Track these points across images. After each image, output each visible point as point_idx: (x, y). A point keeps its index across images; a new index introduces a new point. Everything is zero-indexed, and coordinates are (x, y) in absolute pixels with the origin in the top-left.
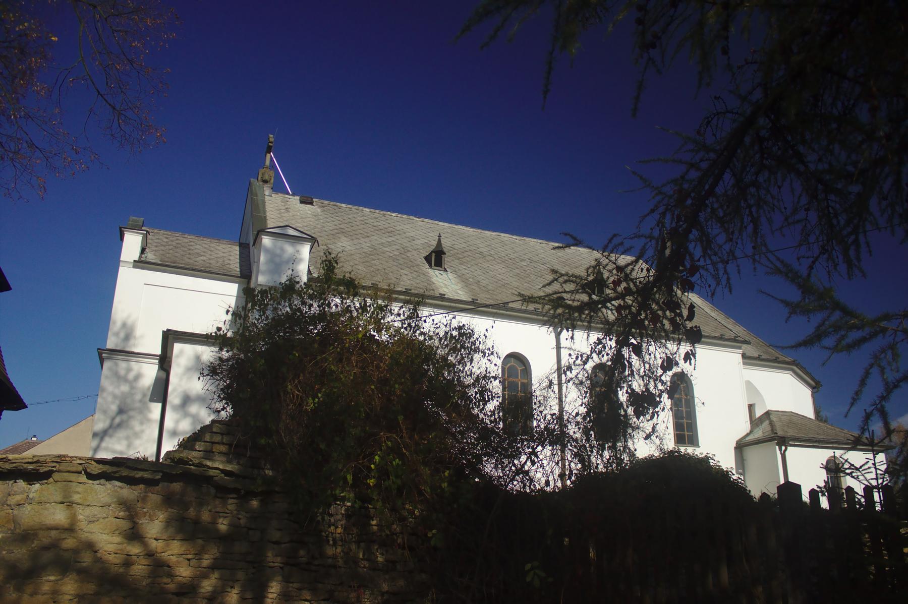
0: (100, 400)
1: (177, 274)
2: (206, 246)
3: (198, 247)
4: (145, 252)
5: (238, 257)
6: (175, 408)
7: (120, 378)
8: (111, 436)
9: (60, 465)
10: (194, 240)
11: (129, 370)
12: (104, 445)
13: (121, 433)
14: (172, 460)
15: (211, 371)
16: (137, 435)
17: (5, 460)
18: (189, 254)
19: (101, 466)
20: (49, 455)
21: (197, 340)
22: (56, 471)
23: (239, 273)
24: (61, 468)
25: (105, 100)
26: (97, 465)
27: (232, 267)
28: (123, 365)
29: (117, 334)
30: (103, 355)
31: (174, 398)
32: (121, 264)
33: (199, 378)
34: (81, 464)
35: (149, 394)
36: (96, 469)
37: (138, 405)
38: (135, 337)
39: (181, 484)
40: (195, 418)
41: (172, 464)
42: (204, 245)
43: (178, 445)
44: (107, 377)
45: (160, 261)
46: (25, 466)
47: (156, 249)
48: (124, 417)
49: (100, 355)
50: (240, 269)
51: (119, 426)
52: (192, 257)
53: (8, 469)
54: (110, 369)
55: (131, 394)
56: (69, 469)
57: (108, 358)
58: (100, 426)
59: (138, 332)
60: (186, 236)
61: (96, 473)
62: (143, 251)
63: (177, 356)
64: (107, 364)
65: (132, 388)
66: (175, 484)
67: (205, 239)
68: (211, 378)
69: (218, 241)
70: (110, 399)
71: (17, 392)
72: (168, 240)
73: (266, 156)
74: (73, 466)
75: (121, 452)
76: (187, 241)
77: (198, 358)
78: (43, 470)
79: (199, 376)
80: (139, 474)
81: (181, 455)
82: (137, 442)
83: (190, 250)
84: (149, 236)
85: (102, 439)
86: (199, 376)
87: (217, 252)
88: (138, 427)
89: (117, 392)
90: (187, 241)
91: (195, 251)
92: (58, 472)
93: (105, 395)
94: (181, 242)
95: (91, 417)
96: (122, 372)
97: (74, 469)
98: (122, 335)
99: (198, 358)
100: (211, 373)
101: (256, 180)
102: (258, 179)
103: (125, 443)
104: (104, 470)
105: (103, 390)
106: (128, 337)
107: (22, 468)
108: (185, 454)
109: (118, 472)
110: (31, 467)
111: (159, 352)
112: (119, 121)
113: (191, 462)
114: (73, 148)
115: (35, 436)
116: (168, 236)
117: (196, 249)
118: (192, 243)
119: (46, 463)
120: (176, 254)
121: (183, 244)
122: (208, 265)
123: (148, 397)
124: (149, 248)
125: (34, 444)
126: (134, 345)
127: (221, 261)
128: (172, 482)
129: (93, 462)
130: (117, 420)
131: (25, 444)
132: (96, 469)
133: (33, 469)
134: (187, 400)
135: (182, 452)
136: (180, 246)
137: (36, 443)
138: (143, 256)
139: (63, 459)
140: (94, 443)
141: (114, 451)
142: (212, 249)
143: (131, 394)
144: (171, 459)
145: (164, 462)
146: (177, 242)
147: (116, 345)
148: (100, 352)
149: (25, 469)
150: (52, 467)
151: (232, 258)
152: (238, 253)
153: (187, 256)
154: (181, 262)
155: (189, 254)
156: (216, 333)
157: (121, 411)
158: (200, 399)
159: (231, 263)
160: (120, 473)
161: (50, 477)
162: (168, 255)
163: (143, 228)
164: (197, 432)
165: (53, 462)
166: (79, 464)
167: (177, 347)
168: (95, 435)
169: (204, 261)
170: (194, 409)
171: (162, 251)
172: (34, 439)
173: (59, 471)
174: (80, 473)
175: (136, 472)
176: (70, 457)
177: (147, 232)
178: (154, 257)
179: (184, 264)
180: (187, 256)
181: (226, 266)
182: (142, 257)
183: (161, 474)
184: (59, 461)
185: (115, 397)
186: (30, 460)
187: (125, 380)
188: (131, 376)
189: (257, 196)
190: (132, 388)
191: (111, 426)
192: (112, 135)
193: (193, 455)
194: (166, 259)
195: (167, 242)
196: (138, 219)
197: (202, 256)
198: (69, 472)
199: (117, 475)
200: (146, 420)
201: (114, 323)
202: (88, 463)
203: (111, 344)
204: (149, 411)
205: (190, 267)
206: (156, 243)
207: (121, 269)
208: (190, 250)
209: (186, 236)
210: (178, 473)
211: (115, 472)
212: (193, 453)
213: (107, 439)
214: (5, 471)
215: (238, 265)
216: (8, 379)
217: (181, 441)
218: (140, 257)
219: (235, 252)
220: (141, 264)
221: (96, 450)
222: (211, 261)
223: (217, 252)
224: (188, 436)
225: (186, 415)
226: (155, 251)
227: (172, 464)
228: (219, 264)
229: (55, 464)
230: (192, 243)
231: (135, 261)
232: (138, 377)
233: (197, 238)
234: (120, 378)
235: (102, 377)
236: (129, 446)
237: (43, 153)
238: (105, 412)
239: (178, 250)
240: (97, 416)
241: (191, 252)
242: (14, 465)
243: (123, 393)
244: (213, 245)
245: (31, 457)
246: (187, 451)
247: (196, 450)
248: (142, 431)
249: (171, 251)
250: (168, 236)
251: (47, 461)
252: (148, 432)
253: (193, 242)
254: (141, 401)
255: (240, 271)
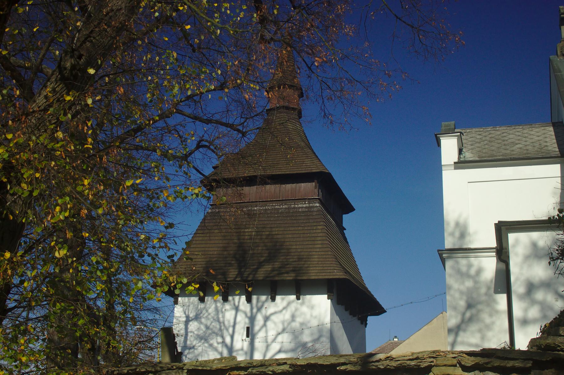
0: (448, 298)
1: (531, 165)
2: (519, 134)
3: (511, 136)
4: (462, 152)
5: (554, 137)
6: (522, 297)
7: (463, 275)
8: (465, 331)
9: (437, 360)
10: (506, 131)
11: (470, 266)
12: (459, 339)
13: (474, 327)
14: (539, 347)
15: (560, 254)
16: (488, 327)
17: (390, 358)
18: (505, 145)
19: (472, 358)
20: (425, 352)
21: (525, 227)
22: (434, 366)
23: (558, 153)
24: (438, 362)
25: (403, 22)
26: (469, 357)
27: (550, 148)
28: (463, 262)
29: (452, 234)
30: (444, 255)
31: (518, 287)
32: (443, 168)
33: (550, 263)
34: (455, 358)
35: (493, 286)
36: (469, 361)
37: (484, 298)
38: (469, 234)
39: (553, 370)
40: (544, 306)
41: (539, 351)
42: (517, 133)
43: (541, 332)
44: (450, 276)
45: (479, 158)
46: (408, 362)
47: (473, 147)
48: (474, 311)
49: (441, 255)
50: (559, 148)
51: (471, 319)
52: (508, 147)
53: (394, 366)
54: (453, 268)
55: (476, 288)
56: (445, 363)
57: (449, 258)
58: (453, 322)
59: (471, 229)
60: (498, 129)
61: (470, 365)
62: (460, 151)
63: (514, 246)
64: (449, 264)
65: (476, 282)
66: (546, 371)
67: (517, 127)
68: (562, 261)
69: (530, 126)
70: (457, 295)
71: (376, 299)
72: (481, 137)
73: (561, 29)
74: (448, 360)
75: (477, 346)
76: (499, 133)
77: (534, 245)
78: (423, 365)
79: (550, 260)
80: (510, 364)
81: (548, 342)
82: (490, 334)
83: (504, 141)
84: (463, 137)
85: (457, 334)
86: (550, 260)
87: (531, 137)
88: (488, 320)
89: (462, 288)
90: (499, 133)
91: (510, 141)
92: (436, 366)
93: (452, 292)
94: (494, 135)
95: (441, 314)
96: (464, 269)
97: (449, 363)
98: (457, 234)
99: (534, 245)
100: (560, 256)
101: (556, 56)
102: (557, 55)
103: (478, 336)
104: (477, 361)
105: (450, 288)
106: (463, 235)
107: (405, 365)
108: (550, 340)
109: (490, 363)
110: (413, 363)
111: (494, 244)
112: (419, 37)
113: (559, 348)
114: (385, 74)
115: (396, 337)
116: (480, 133)
117: (510, 139)
118: (505, 134)
119: (424, 359)
120: (492, 147)
121: (497, 137)
122: (525, 152)
123: (492, 290)
124: (465, 147)
125: (396, 345)
126: (470, 242)
127: (537, 145)
128: (543, 370)
129: (465, 355)
130: (468, 315)
131: (389, 345)
132: (469, 362)
133: (415, 365)
134: (531, 288)
135: (546, 338)
136: (493, 139)
137: (398, 343)
138: (461, 156)
139: (437, 354)
140: (451, 339)
141: (470, 345)
142: (526, 135)
143: (476, 288)
144: (537, 346)
145: (531, 350)
146: (490, 136)
147: (454, 244)
148: (441, 252)
149: (408, 365)
150: (430, 362)
151: (547, 140)
152: (553, 133)
153: (503, 147)
154: (498, 154)
155: (505, 145)
156: (558, 215)
157: (469, 306)
158: (546, 285)
159: (548, 144)
160: (492, 364)
161: (430, 371)
162: (484, 151)
163: (456, 130)
164: (558, 317)
165: (430, 357)
166: (453, 358)
167: (512, 237)
168: (450, 331)
169: (521, 148)
170: (539, 295)
171: (478, 148)
172: (396, 340)
173: (437, 366)
174: (455, 366)
175: (507, 361)
176: (443, 352)
177: (461, 133)
178: (472, 155)
179: (502, 155)
180: (503, 147)
181: (544, 148)
182: (461, 158)
183: (532, 362)
184: (435, 356)
185: (462, 293)
186: (411, 357)
187: (467, 275)
188: (473, 271)
189: (560, 71)
190: (476, 282)
191: (463, 321)
192: (416, 52)
193: (559, 341)
194: (484, 155)
195: (480, 139)
196: (449, 123)
197: (517, 144)
198: (445, 365)
199: (489, 366)
200: (495, 312)
201: (448, 224)
202: (461, 356)
203: (449, 243)
204: (495, 301)
205: (508, 157)
206: (471, 141)
207: (444, 173)
208: (504, 141)
209: (498, 129)
210: (548, 359)
211: (487, 363)
212: (559, 339)
213: (461, 334)
214: (393, 368)
215: (556, 145)
216: (366, 289)
217: (543, 327)
218: (459, 158)
219: (549, 133)
220: (461, 164)
221: (453, 344)
222: (528, 147)
223: (531, 137)
224: (549, 322)
225: (533, 302)
226: (472, 149)
227: (539, 351)
228: (536, 149)
229: (432, 359)
230: (505, 134)
231: (455, 163)
232: (479, 271)
233: (508, 128)
234: (463, 275)
235: (447, 276)
236: (483, 338)
237: (362, 84)
238: (455, 308)
239: (493, 144)
240: (449, 312)
241: (506, 142)
242: (399, 362)
243: (468, 289)
244: (525, 131)
245: (410, 354)
246: (552, 337)
247: (561, 336)
248: (493, 323)
249: (487, 146)
250: (480, 133)
251: (425, 356)
252: (498, 323)
253: (506, 133)
254: (486, 294)
255: (560, 151)
